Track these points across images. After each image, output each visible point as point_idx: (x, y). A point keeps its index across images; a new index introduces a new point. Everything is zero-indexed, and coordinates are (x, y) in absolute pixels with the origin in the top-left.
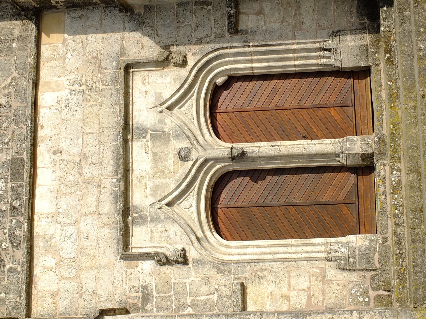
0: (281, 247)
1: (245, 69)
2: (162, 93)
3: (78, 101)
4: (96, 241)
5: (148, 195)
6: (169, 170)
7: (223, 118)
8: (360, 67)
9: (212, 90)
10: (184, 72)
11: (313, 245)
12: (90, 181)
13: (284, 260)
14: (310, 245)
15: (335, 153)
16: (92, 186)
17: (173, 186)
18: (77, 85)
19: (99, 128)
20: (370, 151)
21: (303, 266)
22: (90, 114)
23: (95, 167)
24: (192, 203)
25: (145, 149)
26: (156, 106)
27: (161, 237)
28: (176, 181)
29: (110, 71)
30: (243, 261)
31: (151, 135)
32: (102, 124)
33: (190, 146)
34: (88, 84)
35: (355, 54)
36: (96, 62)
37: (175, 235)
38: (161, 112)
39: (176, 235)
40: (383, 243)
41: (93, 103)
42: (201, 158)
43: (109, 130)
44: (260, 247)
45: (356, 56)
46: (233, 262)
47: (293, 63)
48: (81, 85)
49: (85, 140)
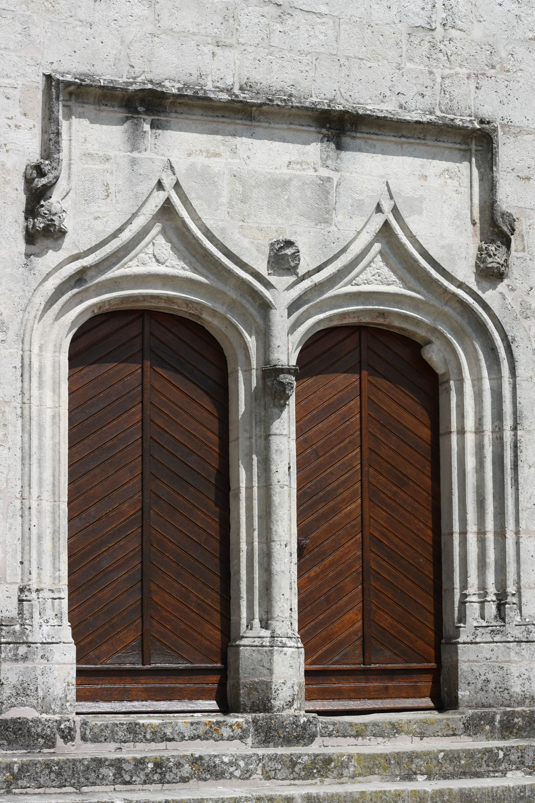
0: (54, 476)
1: (461, 416)
2: (420, 214)
3: (410, 14)
4: (90, 20)
5: (192, 159)
6: (249, 215)
7: (346, 355)
8: (455, 688)
9: (414, 334)
10: (465, 272)
11: (54, 556)
12: (231, 20)
13: (27, 483)
14: (54, 547)
15: (272, 618)
16: (219, 25)
17: (212, 222)
18: (444, 15)
19: (348, 58)
20: (277, 703)
21: (10, 528)
22: (381, 39)
23: (263, 39)
24: (167, 264)
25: (298, 163)
26: (392, 198)
27: (92, 181)
28: (223, 230)
29: (472, 98)
30: (26, 379)
31: (329, 179)
32: (356, 66)
33: (301, 271)
34: (446, 43)
35: (490, 676)
36: (493, 67)
37: (97, 215)
38: (379, 209)
39: (96, 219)
40: (59, 729)
41: (404, 48)
42: (273, 296)
43: (343, 80)
44: (54, 423)
45: (483, 678)
46: (27, 353)
47: (472, 528)
48: (444, 25)
49: (323, 20)
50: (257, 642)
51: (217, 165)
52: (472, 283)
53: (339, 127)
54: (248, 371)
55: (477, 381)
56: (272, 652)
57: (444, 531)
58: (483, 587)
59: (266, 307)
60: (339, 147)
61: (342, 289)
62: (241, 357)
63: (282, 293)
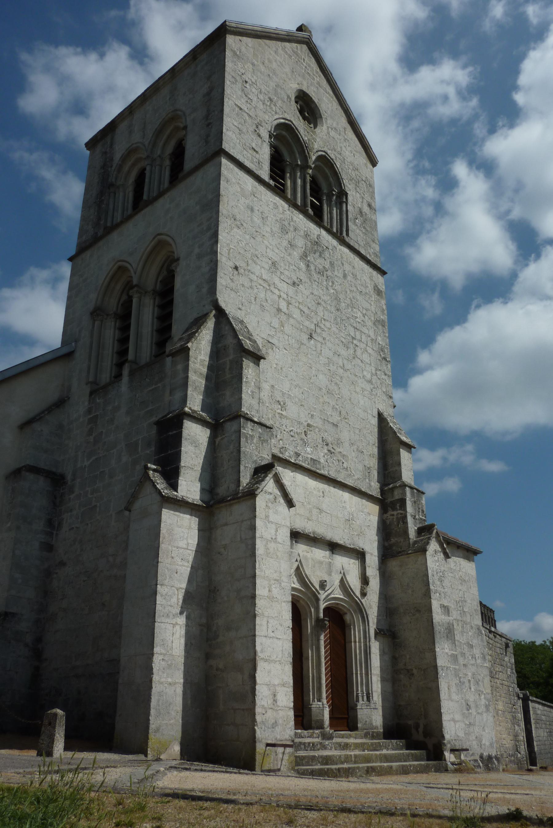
8: (357, 723)
10: (358, 593)
35: (367, 720)
50: (318, 706)
51: (309, 555)
52: (318, 588)
53: (334, 547)
54: (311, 619)
55: (359, 626)
56: (323, 710)
57: (348, 673)
58: (362, 691)
59: (318, 600)
60: (333, 553)
61: (332, 596)
62: (309, 615)
63: (322, 596)
